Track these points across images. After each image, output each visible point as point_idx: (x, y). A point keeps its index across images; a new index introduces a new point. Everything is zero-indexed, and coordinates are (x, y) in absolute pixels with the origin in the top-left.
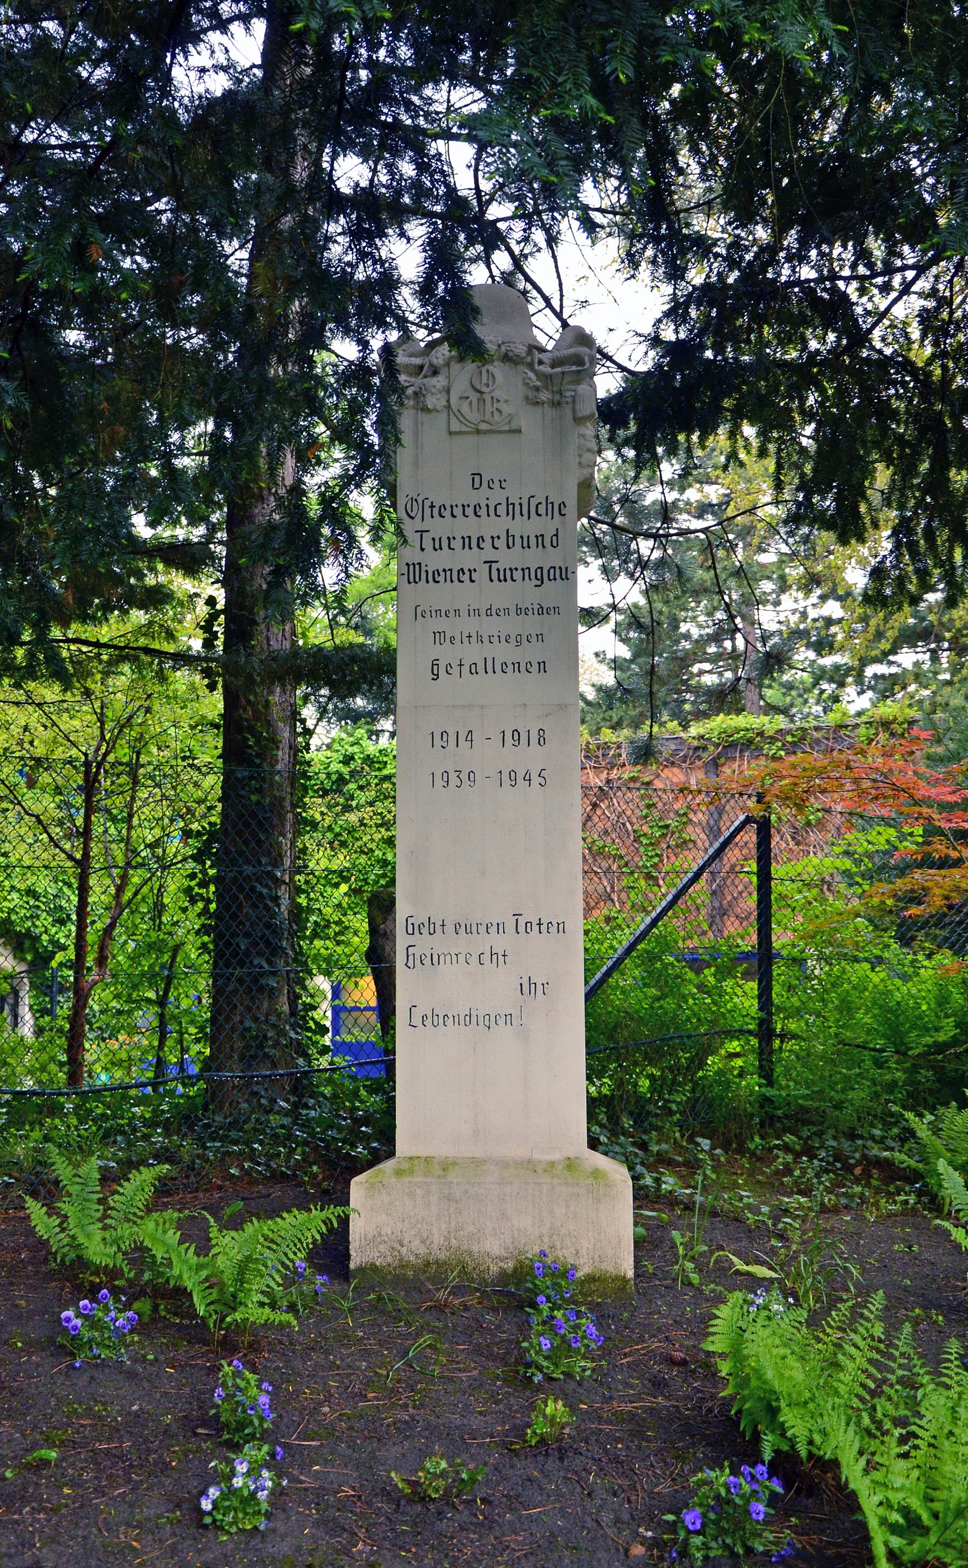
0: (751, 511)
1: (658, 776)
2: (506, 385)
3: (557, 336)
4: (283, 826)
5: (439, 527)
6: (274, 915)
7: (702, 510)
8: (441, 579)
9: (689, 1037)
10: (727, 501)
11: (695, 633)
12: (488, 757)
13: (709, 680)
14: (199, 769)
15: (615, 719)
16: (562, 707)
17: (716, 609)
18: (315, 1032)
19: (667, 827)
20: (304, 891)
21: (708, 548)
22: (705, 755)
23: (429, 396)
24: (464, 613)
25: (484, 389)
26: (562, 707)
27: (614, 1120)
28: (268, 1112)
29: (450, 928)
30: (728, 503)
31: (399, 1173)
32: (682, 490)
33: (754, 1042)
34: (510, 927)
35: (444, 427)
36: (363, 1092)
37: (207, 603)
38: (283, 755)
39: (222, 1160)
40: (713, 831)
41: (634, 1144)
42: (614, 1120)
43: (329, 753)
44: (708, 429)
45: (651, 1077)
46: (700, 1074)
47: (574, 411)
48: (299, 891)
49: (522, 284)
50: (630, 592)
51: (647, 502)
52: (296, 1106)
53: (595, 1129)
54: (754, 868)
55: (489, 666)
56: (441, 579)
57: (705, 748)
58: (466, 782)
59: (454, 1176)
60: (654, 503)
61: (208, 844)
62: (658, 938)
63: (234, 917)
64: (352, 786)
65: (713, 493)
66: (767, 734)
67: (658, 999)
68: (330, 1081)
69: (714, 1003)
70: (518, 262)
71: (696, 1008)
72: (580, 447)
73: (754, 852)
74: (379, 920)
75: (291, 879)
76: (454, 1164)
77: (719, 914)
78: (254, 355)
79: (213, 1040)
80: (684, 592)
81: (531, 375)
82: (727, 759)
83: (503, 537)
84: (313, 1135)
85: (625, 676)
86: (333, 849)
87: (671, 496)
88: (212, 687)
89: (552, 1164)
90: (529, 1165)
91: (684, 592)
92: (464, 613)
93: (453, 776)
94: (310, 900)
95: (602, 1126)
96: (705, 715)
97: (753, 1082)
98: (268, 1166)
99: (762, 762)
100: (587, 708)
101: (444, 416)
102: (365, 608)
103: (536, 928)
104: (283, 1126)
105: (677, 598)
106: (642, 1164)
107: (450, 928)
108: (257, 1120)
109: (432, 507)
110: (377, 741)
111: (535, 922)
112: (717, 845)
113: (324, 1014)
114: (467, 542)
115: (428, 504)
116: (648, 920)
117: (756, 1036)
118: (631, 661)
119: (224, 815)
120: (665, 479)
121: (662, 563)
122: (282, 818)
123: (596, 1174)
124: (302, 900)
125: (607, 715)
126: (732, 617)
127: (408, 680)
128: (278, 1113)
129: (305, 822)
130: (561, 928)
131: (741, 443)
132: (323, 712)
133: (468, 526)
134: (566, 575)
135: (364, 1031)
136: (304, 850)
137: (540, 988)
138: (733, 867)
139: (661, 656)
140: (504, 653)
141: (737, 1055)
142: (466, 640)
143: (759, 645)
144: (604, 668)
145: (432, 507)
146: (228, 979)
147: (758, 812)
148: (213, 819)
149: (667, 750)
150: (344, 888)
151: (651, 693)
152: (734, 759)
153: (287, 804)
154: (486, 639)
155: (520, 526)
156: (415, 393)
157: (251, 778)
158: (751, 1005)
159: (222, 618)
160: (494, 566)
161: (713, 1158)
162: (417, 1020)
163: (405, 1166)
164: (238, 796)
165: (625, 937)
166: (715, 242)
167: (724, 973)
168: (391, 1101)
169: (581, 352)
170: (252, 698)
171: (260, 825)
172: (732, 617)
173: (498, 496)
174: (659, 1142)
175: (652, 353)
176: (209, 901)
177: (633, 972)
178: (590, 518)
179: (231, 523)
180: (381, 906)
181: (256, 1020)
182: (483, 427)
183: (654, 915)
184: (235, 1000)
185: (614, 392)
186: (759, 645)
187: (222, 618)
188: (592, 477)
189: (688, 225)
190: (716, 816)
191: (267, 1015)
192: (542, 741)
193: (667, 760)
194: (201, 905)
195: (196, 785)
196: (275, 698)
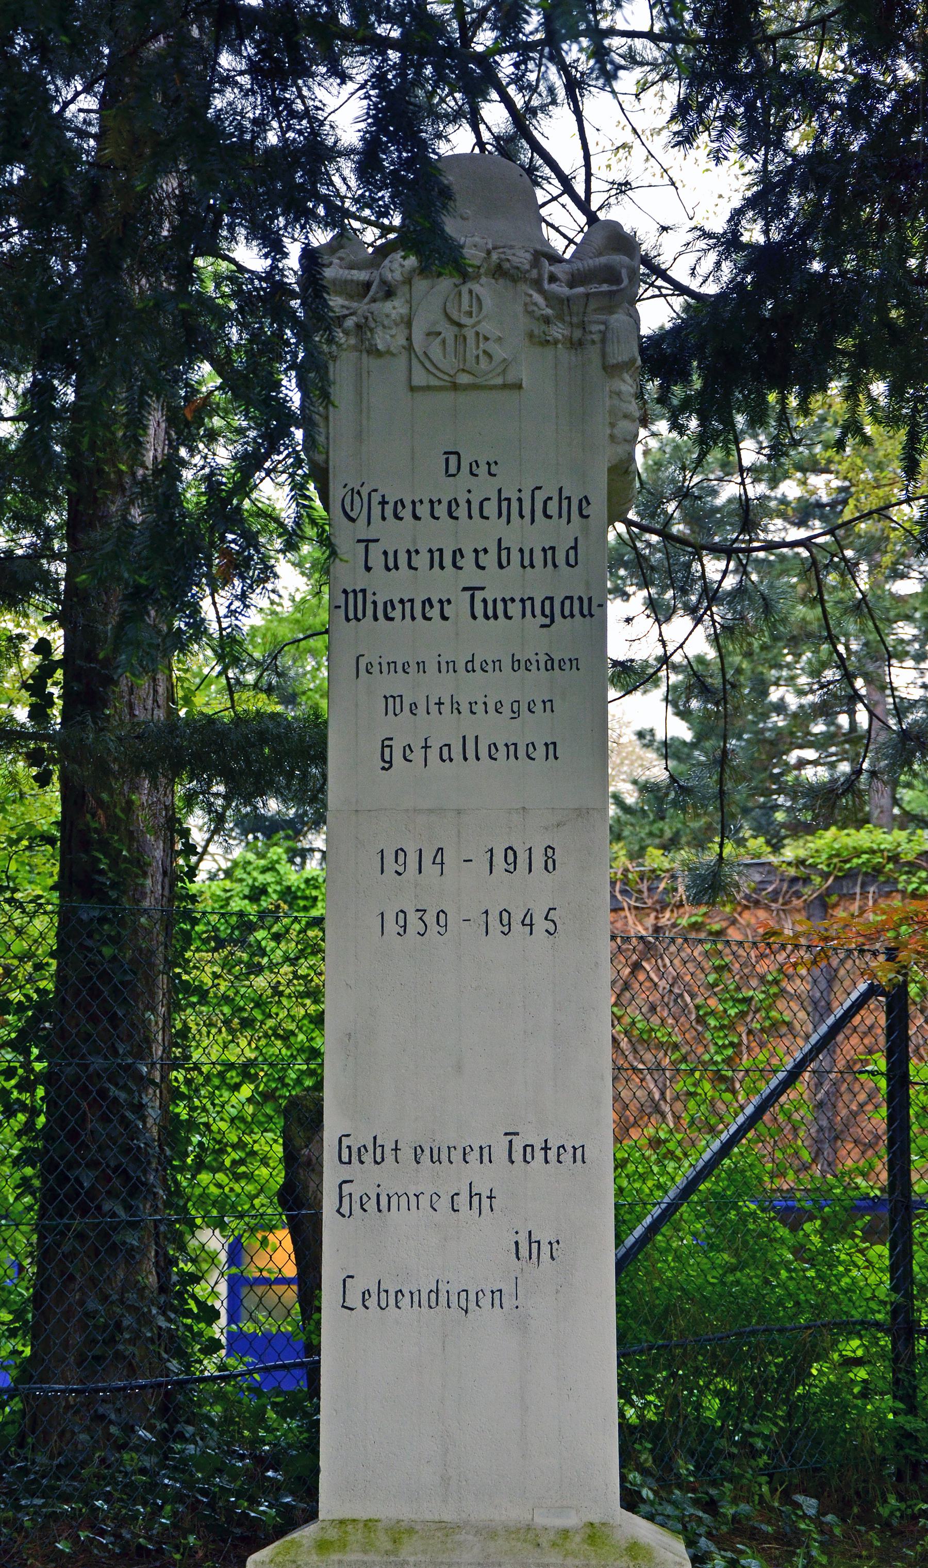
0: (882, 512)
1: (734, 922)
2: (500, 316)
3: (578, 239)
4: (153, 995)
5: (394, 535)
6: (134, 1134)
7: (805, 512)
8: (397, 614)
9: (781, 1331)
10: (843, 496)
11: (793, 702)
12: (467, 889)
13: (815, 775)
14: (20, 905)
15: (668, 834)
16: (582, 813)
17: (824, 665)
18: (197, 1318)
19: (748, 1000)
20: (183, 1097)
21: (813, 570)
22: (807, 890)
23: (379, 332)
24: (432, 667)
25: (465, 320)
26: (582, 813)
27: (664, 1461)
28: (121, 1447)
29: (406, 1154)
30: (845, 502)
31: (323, 1546)
32: (774, 483)
33: (885, 1341)
34: (500, 1152)
35: (403, 377)
36: (271, 1414)
37: (36, 650)
38: (152, 884)
39: (44, 1527)
40: (819, 1008)
41: (696, 1502)
42: (664, 1461)
43: (228, 884)
44: (814, 383)
45: (722, 1394)
46: (800, 1390)
47: (604, 355)
48: (176, 1095)
49: (526, 155)
50: (690, 638)
51: (720, 501)
52: (164, 1436)
53: (635, 1477)
54: (883, 1065)
55: (469, 749)
56: (397, 614)
57: (807, 880)
58: (433, 928)
59: (409, 1552)
60: (730, 501)
61: (33, 1022)
62: (730, 1172)
63: (73, 1136)
64: (260, 934)
65: (822, 486)
66: (904, 858)
67: (733, 1269)
68: (220, 1397)
69: (820, 1277)
70: (521, 120)
71: (792, 1285)
72: (612, 412)
73: (882, 1040)
74: (299, 1142)
75: (164, 1077)
76: (411, 1531)
77: (829, 1138)
78: (103, 264)
79: (35, 1333)
80: (775, 639)
81: (538, 298)
82: (842, 897)
83: (493, 550)
84: (190, 1484)
85: (683, 768)
86: (231, 1031)
87: (756, 490)
88: (43, 780)
89: (565, 1533)
90: (528, 1534)
91: (775, 639)
92: (432, 667)
93: (413, 918)
94: (193, 1109)
95: (644, 1472)
96: (810, 829)
97: (884, 1406)
98: (118, 1536)
99: (897, 902)
100: (624, 817)
101: (402, 360)
102: (285, 661)
103: (540, 1155)
104: (143, 1471)
105: (764, 647)
106: (709, 1535)
107: (406, 1154)
108: (103, 1461)
109: (383, 503)
110: (303, 863)
111: (539, 1145)
112: (823, 1029)
113: (214, 1289)
114: (436, 558)
115: (376, 498)
116: (716, 1145)
117: (887, 1332)
118: (693, 745)
119: (60, 978)
120: (746, 463)
121: (740, 591)
122: (151, 984)
123: (634, 1549)
124: (182, 1111)
125: (655, 828)
126: (849, 677)
127: (345, 768)
128: (136, 1449)
129: (187, 988)
130: (579, 1154)
131: (864, 408)
132: (218, 821)
133: (439, 534)
134: (591, 612)
135: (275, 1317)
136: (184, 1032)
137: (545, 1249)
138: (849, 1066)
139: (740, 738)
140: (495, 729)
141: (858, 1362)
142: (434, 709)
143: (892, 722)
144: (651, 755)
145: (383, 503)
146: (63, 1234)
147: (886, 975)
148: (42, 984)
149: (746, 883)
150: (246, 1091)
151: (722, 793)
152: (852, 897)
153: (159, 961)
154: (465, 708)
155: (518, 534)
156: (358, 326)
157: (103, 920)
158: (879, 1281)
159: (59, 674)
160: (479, 595)
161: (824, 1529)
162: (354, 1299)
163: (333, 1534)
164: (82, 947)
165: (682, 1173)
166: (832, 86)
167: (835, 1230)
168: (314, 1427)
169: (617, 262)
170: (105, 796)
171: (116, 992)
172: (849, 677)
173: (484, 487)
174: (735, 1501)
175: (727, 267)
176: (34, 1112)
177: (692, 1224)
178: (629, 523)
179: (74, 528)
180: (302, 1118)
181: (105, 1298)
182: (464, 379)
183: (725, 1136)
184: (71, 1268)
185: (668, 326)
186: (892, 722)
187: (59, 674)
188: (631, 458)
189: (790, 58)
190: (823, 984)
191: (123, 1291)
192: (550, 864)
193: (747, 897)
194: (22, 1117)
195: (20, 932)
196: (141, 798)
